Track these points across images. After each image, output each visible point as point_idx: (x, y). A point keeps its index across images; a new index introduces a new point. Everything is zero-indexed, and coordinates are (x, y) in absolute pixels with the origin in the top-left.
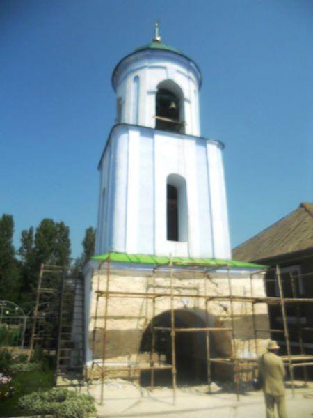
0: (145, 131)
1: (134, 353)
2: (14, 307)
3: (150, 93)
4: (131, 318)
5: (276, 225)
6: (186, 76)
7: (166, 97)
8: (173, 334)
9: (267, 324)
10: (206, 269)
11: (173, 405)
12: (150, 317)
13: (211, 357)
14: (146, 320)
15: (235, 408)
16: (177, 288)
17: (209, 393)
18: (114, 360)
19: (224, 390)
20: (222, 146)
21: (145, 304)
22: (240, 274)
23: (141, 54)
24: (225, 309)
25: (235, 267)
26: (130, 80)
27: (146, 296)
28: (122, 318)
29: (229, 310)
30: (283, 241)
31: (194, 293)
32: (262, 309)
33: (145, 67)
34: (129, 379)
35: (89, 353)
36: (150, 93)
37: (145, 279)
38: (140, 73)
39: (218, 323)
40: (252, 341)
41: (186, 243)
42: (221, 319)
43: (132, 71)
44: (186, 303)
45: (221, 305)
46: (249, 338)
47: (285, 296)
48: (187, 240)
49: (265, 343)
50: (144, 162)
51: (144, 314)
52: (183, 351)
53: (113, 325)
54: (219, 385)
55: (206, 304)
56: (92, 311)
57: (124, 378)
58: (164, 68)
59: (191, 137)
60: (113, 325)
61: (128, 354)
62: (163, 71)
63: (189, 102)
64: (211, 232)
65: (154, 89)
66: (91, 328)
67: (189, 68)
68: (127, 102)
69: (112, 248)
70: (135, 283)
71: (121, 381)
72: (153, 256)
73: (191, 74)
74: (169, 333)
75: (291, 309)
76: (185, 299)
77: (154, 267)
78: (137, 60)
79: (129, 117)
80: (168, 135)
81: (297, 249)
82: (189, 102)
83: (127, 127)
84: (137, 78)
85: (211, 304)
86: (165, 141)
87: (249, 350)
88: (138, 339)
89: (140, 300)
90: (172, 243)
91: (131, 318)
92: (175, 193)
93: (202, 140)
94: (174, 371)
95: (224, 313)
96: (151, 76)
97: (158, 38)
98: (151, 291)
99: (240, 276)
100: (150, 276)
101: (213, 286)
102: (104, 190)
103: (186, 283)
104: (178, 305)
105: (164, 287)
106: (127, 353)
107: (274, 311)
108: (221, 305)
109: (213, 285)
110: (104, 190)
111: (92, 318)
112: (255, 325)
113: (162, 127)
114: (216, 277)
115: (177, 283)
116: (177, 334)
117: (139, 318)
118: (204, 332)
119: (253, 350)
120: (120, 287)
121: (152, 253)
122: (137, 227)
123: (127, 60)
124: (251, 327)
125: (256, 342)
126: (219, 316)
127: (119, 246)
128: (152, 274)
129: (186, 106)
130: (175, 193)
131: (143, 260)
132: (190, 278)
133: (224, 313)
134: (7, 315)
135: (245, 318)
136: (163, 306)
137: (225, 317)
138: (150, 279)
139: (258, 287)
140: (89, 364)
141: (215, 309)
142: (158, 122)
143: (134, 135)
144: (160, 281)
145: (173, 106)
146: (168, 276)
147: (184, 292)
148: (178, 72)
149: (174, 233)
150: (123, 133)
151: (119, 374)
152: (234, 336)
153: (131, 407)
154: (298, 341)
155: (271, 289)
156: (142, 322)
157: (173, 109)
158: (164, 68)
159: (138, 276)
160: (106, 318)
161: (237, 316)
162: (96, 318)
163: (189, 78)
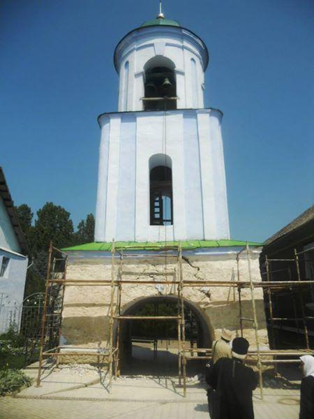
1: (105, 340)
3: (137, 75)
4: (102, 305)
6: (179, 47)
7: (158, 75)
11: (184, 397)
16: (151, 274)
18: (84, 346)
21: (116, 294)
22: (228, 255)
23: (129, 38)
28: (94, 305)
31: (170, 279)
32: (259, 294)
33: (132, 51)
36: (137, 75)
37: (117, 267)
42: (202, 306)
43: (123, 59)
44: (160, 290)
45: (203, 291)
49: (235, 337)
50: (126, 147)
52: (148, 336)
53: (84, 313)
57: (92, 364)
58: (152, 45)
60: (84, 313)
61: (99, 340)
62: (151, 49)
65: (142, 69)
67: (183, 37)
70: (105, 271)
71: (89, 366)
73: (186, 44)
76: (159, 286)
78: (127, 45)
80: (150, 116)
82: (183, 74)
91: (102, 305)
92: (161, 177)
96: (138, 59)
97: (161, 15)
101: (193, 271)
103: (161, 269)
104: (150, 291)
105: (136, 274)
106: (97, 340)
108: (203, 291)
109: (193, 269)
112: (241, 313)
113: (151, 106)
114: (197, 261)
115: (151, 269)
120: (91, 276)
122: (119, 211)
123: (120, 48)
124: (238, 312)
126: (200, 303)
129: (179, 78)
130: (161, 177)
131: (222, 244)
133: (207, 299)
134: (37, 303)
137: (207, 304)
141: (192, 295)
144: (132, 267)
145: (167, 82)
146: (141, 262)
147: (158, 278)
148: (167, 44)
149: (157, 218)
150: (106, 123)
151: (90, 359)
153: (59, 391)
154: (303, 329)
158: (152, 45)
163: (183, 48)
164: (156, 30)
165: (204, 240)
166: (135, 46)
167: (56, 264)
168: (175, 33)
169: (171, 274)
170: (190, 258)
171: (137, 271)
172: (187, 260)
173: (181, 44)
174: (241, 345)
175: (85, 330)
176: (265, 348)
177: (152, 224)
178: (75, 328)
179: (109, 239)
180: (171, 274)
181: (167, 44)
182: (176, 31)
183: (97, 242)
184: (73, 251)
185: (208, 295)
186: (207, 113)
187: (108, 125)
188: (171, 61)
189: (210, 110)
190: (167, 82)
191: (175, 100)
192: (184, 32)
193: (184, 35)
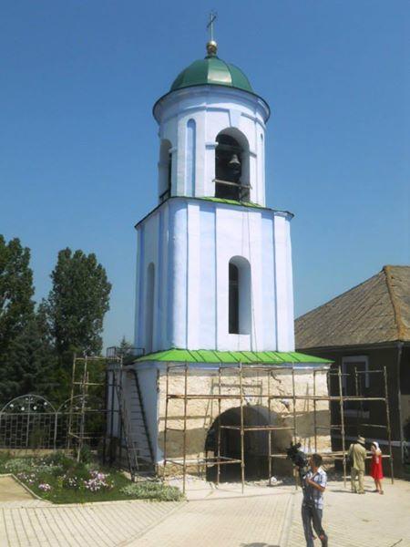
0: (206, 204)
2: (42, 402)
3: (209, 147)
4: (196, 417)
5: (351, 292)
8: (242, 433)
9: (328, 420)
10: (271, 366)
12: (215, 414)
13: (240, 464)
14: (211, 418)
15: (294, 494)
17: (270, 485)
19: (285, 484)
20: (290, 216)
24: (287, 406)
25: (299, 363)
26: (184, 121)
27: (211, 397)
29: (292, 407)
30: (354, 324)
32: (324, 406)
34: (199, 475)
35: (159, 453)
37: (209, 378)
38: (195, 116)
39: (280, 420)
40: (312, 439)
41: (248, 336)
42: (283, 416)
46: (308, 435)
47: (339, 401)
48: (250, 333)
51: (209, 413)
54: (278, 479)
55: (269, 401)
56: (161, 411)
59: (256, 208)
63: (255, 156)
64: (274, 326)
66: (161, 428)
67: (255, 107)
68: (179, 154)
69: (173, 344)
70: (199, 383)
72: (215, 351)
74: (239, 431)
75: (349, 405)
77: (220, 366)
78: (192, 96)
79: (182, 189)
81: (365, 342)
82: (255, 156)
83: (185, 201)
84: (192, 123)
85: (273, 401)
86: (228, 217)
87: (309, 447)
88: (203, 437)
89: (206, 401)
90: (234, 336)
91: (196, 417)
92: (238, 272)
93: (268, 212)
94: (243, 465)
95: (286, 410)
96: (211, 121)
98: (216, 392)
99: (304, 372)
100: (214, 375)
102: (152, 267)
103: (249, 381)
107: (334, 405)
110: (152, 267)
111: (162, 419)
114: (279, 374)
116: (245, 432)
117: (205, 417)
118: (267, 432)
119: (312, 446)
121: (214, 348)
122: (198, 321)
124: (311, 423)
125: (187, 367)
126: (281, 414)
127: (179, 341)
128: (216, 372)
129: (252, 159)
130: (238, 272)
132: (254, 376)
133: (286, 410)
135: (306, 414)
136: (227, 405)
137: (286, 414)
138: (214, 377)
139: (321, 382)
140: (161, 463)
141: (278, 407)
142: (218, 187)
143: (193, 209)
144: (224, 379)
145: (236, 161)
148: (243, 115)
149: (234, 327)
152: (295, 434)
155: (333, 388)
156: (208, 420)
157: (235, 164)
158: (227, 111)
159: (204, 375)
160: (185, 418)
161: (300, 413)
162: (166, 419)
163: (256, 121)
164: (246, 96)
165: (277, 351)
166: (204, 104)
167: (83, 370)
168: (236, 96)
169: (258, 386)
170: (274, 372)
171: (228, 383)
172: (272, 375)
173: (254, 116)
174: (368, 446)
175: (182, 441)
176: (329, 450)
177: (231, 332)
178: (172, 441)
179: (194, 345)
180: (258, 386)
181: (243, 115)
182: (238, 91)
183: (178, 349)
184: (141, 361)
185: (287, 406)
186: (283, 216)
187: (184, 210)
188: (243, 135)
189: (286, 214)
190: (236, 161)
191: (217, 177)
192: (260, 102)
193: (259, 104)
